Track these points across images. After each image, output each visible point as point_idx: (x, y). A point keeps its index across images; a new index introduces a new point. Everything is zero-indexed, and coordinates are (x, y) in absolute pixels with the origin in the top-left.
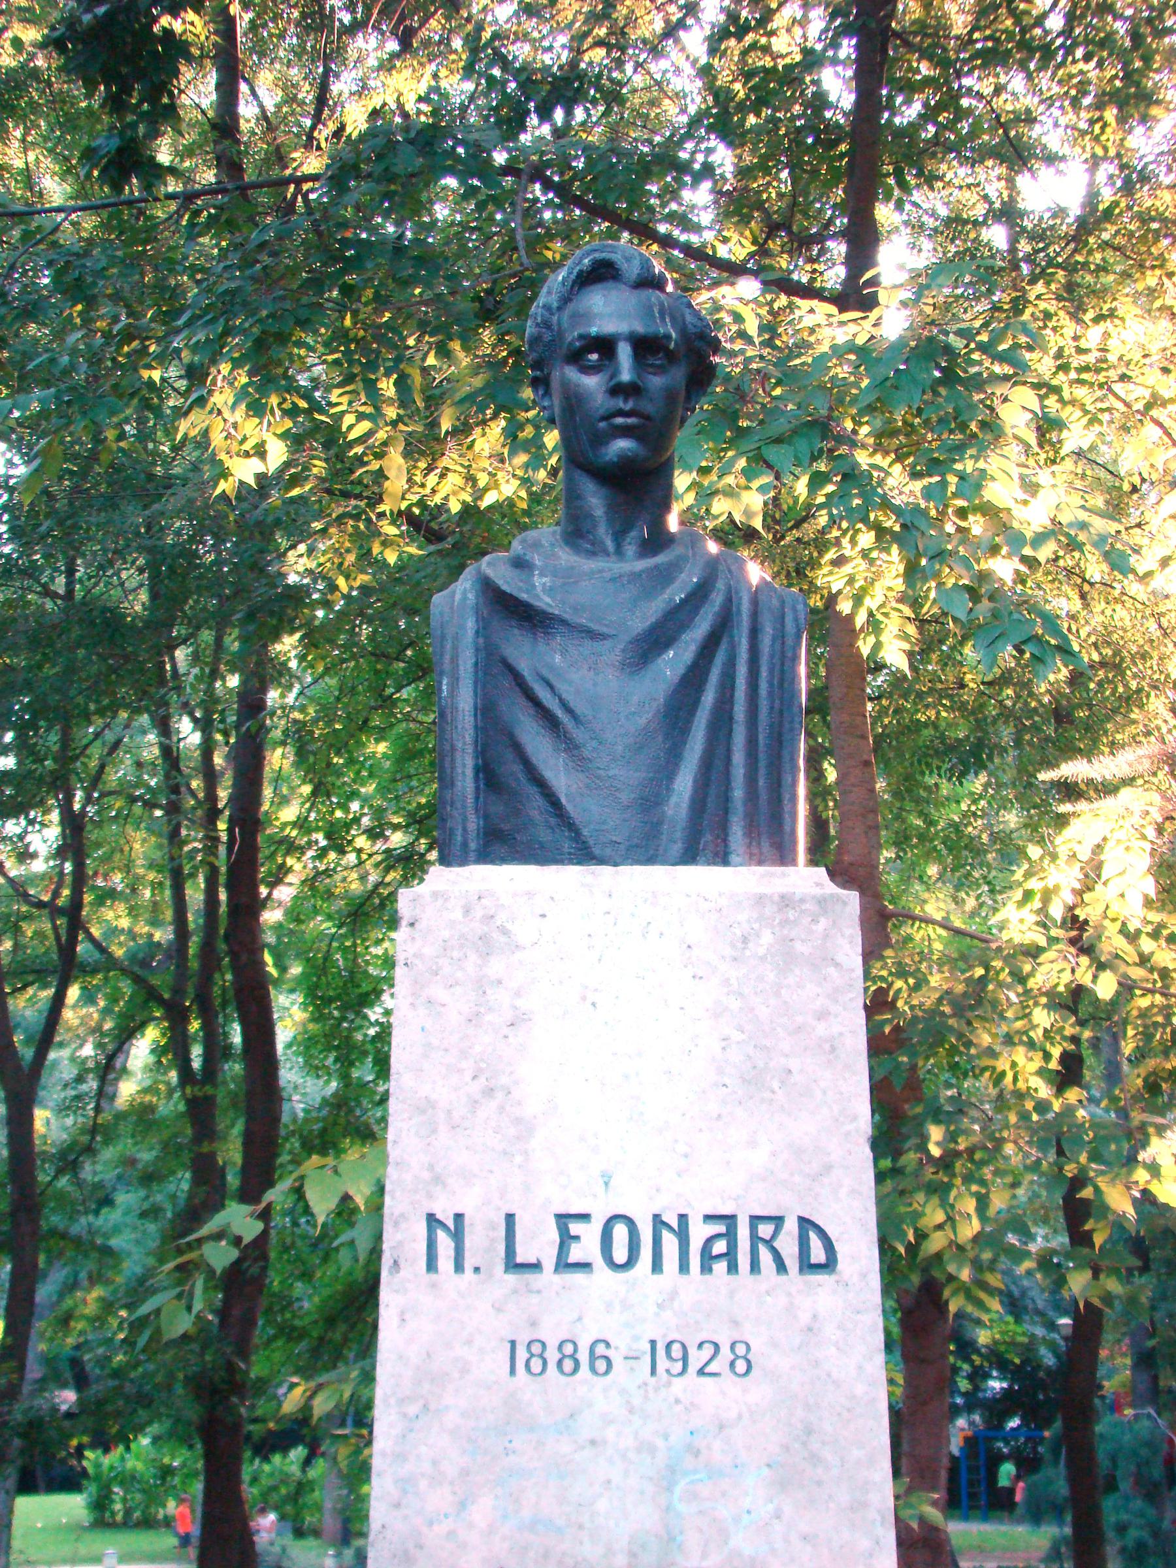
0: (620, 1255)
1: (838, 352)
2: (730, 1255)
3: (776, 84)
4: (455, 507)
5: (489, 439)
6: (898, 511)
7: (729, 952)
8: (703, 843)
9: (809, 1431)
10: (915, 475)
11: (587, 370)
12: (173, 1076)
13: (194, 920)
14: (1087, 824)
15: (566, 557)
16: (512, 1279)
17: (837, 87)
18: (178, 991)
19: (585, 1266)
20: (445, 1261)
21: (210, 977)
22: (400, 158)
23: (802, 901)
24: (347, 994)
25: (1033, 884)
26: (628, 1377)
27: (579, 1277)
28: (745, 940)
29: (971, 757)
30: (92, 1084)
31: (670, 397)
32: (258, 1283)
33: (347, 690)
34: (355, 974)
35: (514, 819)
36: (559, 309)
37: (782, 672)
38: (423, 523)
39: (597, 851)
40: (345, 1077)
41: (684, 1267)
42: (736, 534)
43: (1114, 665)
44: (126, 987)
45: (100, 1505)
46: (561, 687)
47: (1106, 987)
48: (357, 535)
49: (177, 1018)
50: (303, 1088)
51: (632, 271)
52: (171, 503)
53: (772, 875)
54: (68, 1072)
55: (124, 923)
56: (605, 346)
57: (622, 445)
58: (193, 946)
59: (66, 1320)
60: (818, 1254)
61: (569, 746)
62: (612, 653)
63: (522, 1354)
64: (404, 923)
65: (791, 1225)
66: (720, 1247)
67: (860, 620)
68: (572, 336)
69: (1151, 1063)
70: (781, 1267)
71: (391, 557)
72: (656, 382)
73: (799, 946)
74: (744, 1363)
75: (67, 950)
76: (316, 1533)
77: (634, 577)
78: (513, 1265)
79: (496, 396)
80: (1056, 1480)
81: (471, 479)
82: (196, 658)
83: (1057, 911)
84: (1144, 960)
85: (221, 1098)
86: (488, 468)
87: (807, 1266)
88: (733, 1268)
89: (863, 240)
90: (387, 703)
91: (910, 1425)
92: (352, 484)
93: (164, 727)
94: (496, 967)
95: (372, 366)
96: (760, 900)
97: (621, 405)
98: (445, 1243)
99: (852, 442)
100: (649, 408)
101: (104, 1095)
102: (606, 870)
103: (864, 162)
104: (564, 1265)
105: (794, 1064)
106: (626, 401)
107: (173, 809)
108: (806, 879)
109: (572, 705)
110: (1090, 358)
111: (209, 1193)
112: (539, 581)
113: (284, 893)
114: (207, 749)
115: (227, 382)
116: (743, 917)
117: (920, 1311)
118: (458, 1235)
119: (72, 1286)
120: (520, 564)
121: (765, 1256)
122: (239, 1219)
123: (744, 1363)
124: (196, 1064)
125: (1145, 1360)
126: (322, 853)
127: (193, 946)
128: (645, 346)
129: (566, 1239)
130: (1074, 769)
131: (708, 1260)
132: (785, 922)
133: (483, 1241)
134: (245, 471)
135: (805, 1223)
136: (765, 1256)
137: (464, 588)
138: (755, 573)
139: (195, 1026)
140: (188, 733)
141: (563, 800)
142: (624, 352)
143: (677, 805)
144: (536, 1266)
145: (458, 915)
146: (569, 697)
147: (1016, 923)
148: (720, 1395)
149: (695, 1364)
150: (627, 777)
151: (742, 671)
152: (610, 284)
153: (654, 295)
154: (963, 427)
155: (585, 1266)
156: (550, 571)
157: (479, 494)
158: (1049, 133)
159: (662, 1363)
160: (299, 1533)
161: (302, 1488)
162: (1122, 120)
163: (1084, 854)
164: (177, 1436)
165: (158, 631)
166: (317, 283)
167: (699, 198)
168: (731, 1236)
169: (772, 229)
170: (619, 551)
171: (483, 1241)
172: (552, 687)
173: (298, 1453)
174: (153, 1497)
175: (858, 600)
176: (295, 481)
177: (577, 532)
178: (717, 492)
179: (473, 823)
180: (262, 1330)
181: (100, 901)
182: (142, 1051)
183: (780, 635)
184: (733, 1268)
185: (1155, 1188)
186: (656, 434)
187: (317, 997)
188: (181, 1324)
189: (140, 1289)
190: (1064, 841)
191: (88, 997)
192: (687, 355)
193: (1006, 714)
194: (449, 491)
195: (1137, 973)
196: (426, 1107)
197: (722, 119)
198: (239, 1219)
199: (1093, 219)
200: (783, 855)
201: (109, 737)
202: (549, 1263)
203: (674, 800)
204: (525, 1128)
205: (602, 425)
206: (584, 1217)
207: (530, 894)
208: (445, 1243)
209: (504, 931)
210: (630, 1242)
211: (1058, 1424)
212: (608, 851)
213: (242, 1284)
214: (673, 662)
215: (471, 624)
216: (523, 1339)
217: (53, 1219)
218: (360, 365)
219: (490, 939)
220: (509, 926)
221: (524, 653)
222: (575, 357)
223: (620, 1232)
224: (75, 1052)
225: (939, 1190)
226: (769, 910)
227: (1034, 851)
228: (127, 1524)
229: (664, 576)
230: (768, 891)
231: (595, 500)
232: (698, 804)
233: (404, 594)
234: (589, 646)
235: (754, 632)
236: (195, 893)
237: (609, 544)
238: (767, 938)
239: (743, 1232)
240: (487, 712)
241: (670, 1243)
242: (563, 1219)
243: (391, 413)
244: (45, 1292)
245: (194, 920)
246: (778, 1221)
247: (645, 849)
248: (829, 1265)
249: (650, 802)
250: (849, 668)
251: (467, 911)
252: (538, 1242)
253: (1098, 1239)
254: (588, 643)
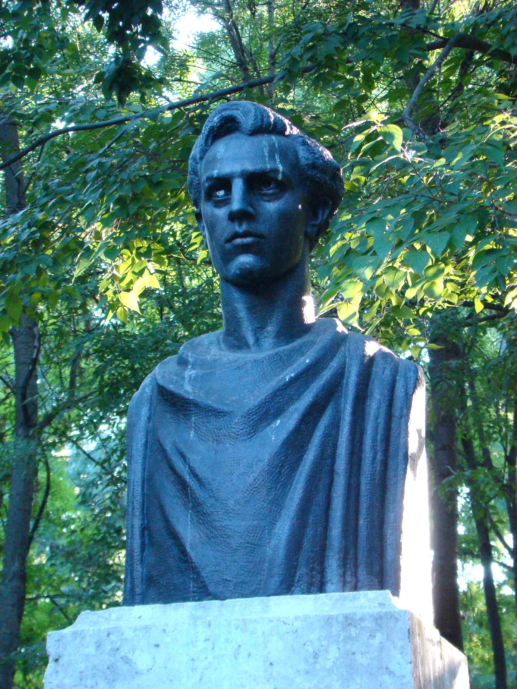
7: (302, 666)
23: (362, 619)
28: (316, 656)
36: (201, 158)
37: (388, 428)
39: (211, 588)
46: (194, 459)
51: (248, 122)
53: (345, 599)
56: (224, 183)
61: (196, 506)
64: (51, 660)
73: (360, 659)
96: (328, 620)
97: (237, 229)
100: (261, 228)
102: (216, 603)
106: (240, 225)
109: (198, 471)
116: (313, 636)
132: (348, 639)
141: (188, 549)
142: (238, 186)
143: (276, 546)
145: (91, 650)
146: (195, 465)
152: (237, 134)
172: (183, 456)
203: (274, 542)
205: (228, 245)
207: (147, 629)
209: (127, 661)
212: (221, 588)
219: (116, 666)
220: (130, 656)
226: (335, 629)
230: (333, 613)
237: (251, 340)
238: (333, 653)
251: (99, 646)
254: (212, 419)
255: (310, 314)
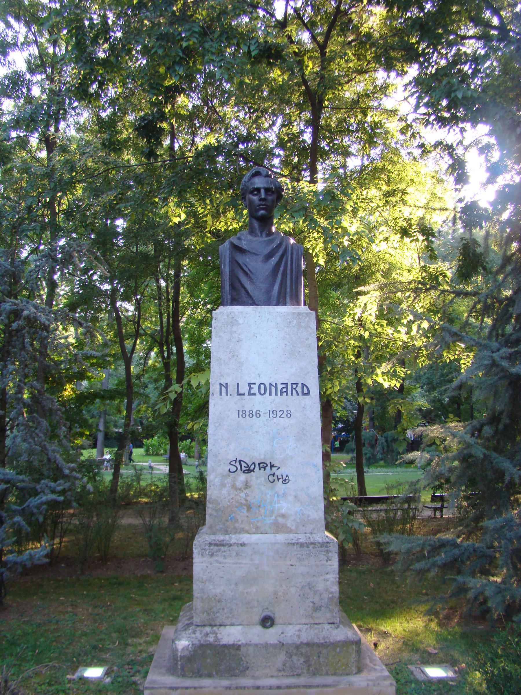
0: (262, 392)
1: (309, 192)
2: (286, 392)
3: (293, 137)
4: (223, 230)
5: (230, 214)
6: (322, 228)
8: (281, 301)
9: (304, 429)
10: (326, 220)
11: (254, 195)
12: (160, 359)
13: (165, 325)
14: (362, 299)
15: (249, 237)
16: (238, 397)
17: (307, 137)
18: (161, 340)
19: (255, 394)
20: (224, 393)
21: (170, 336)
22: (210, 152)
24: (198, 341)
25: (351, 312)
26: (264, 418)
27: (253, 397)
29: (338, 286)
30: (142, 361)
31: (273, 201)
32: (181, 403)
33: (198, 273)
34: (200, 336)
35: (239, 296)
38: (216, 234)
40: (198, 359)
41: (276, 394)
42: (288, 234)
43: (369, 266)
44: (150, 339)
45: (147, 451)
46: (249, 267)
47: (366, 335)
48: (201, 236)
49: (161, 346)
50: (189, 362)
51: (264, 173)
52: (159, 230)
54: (137, 358)
55: (149, 325)
56: (258, 190)
57: (262, 212)
58: (164, 330)
59: (139, 411)
60: (306, 391)
61: (251, 279)
62: (260, 258)
63: (241, 413)
65: (300, 385)
66: (284, 390)
67: (314, 254)
68: (251, 188)
69: (376, 353)
70: (298, 394)
71: (209, 241)
72: (270, 198)
73: (303, 324)
74: (289, 415)
75: (137, 331)
76: (193, 457)
77: (265, 241)
78: (239, 394)
79: (233, 204)
80: (352, 445)
81: (226, 223)
82: (164, 266)
83: (356, 318)
84: (376, 330)
85: (171, 364)
86: (230, 222)
87: (303, 394)
88: (287, 394)
89: (314, 171)
90: (207, 276)
91: (325, 429)
92: (200, 225)
93: (157, 281)
94: (234, 328)
95: (205, 197)
96: (293, 313)
98: (223, 389)
99: (313, 213)
100: (268, 204)
101: (145, 363)
103: (313, 154)
104: (250, 394)
105: (301, 350)
107: (160, 299)
108: (303, 309)
110: (364, 197)
111: (169, 383)
112: (243, 242)
113: (184, 319)
114: (167, 287)
115: (172, 201)
117: (326, 406)
118: (226, 387)
119: (139, 405)
120: (239, 239)
121: (294, 392)
122: (176, 387)
123: (289, 415)
124: (166, 355)
125: (372, 419)
126: (192, 310)
127: (164, 330)
128: (267, 190)
129: (250, 388)
130: (361, 289)
131: (282, 393)
133: (232, 389)
134: (176, 220)
135: (303, 385)
136: (294, 392)
137: (227, 244)
138: (292, 241)
139: (165, 348)
140: (163, 284)
142: (263, 191)
144: (244, 394)
147: (348, 322)
148: (284, 422)
149: (279, 415)
150: (264, 286)
151: (289, 263)
153: (269, 179)
154: (337, 209)
155: (255, 394)
156: (246, 241)
157: (228, 227)
158: (353, 149)
159: (272, 415)
160: (190, 457)
161: (190, 447)
162: (370, 147)
163: (363, 305)
164: (163, 435)
165: (157, 259)
166: (192, 178)
167: (276, 162)
168: (287, 387)
169: (294, 168)
170: (261, 236)
171: (232, 389)
173: (189, 441)
174: (158, 449)
175: (313, 250)
176: (187, 224)
177: (252, 232)
178: (282, 225)
179: (229, 297)
180: (182, 414)
181: (144, 321)
182: (153, 354)
183: (298, 255)
184: (287, 394)
185: (377, 379)
186: (270, 209)
187: (192, 343)
188: (164, 411)
189: (155, 404)
190: (358, 303)
191: (141, 343)
192: (276, 192)
193: (345, 277)
194: (221, 226)
195: (374, 332)
196: (219, 359)
197: (281, 145)
198: (176, 387)
199: (363, 168)
200: (299, 304)
201: (146, 283)
202: (247, 394)
204: (241, 364)
206: (254, 384)
208: (223, 389)
210: (265, 389)
211: (354, 433)
213: (177, 403)
214: (274, 261)
215: (228, 252)
216: (241, 410)
217: (136, 389)
218: (202, 197)
219: (233, 322)
221: (240, 259)
222: (252, 192)
223: (262, 387)
224: (139, 353)
225: (331, 380)
227: (352, 305)
228: (153, 455)
229: (271, 241)
231: (256, 224)
232: (279, 293)
233: (211, 250)
234: (255, 257)
235: (292, 254)
236: (165, 320)
238: (295, 322)
239: (289, 387)
240: (232, 272)
241: (273, 389)
242: (250, 384)
243: (209, 207)
244: (134, 406)
245: (165, 325)
246: (297, 384)
247: (268, 302)
248: (308, 394)
249: (269, 292)
250: (311, 265)
252: (244, 389)
253: (364, 390)
255: (274, 229)
